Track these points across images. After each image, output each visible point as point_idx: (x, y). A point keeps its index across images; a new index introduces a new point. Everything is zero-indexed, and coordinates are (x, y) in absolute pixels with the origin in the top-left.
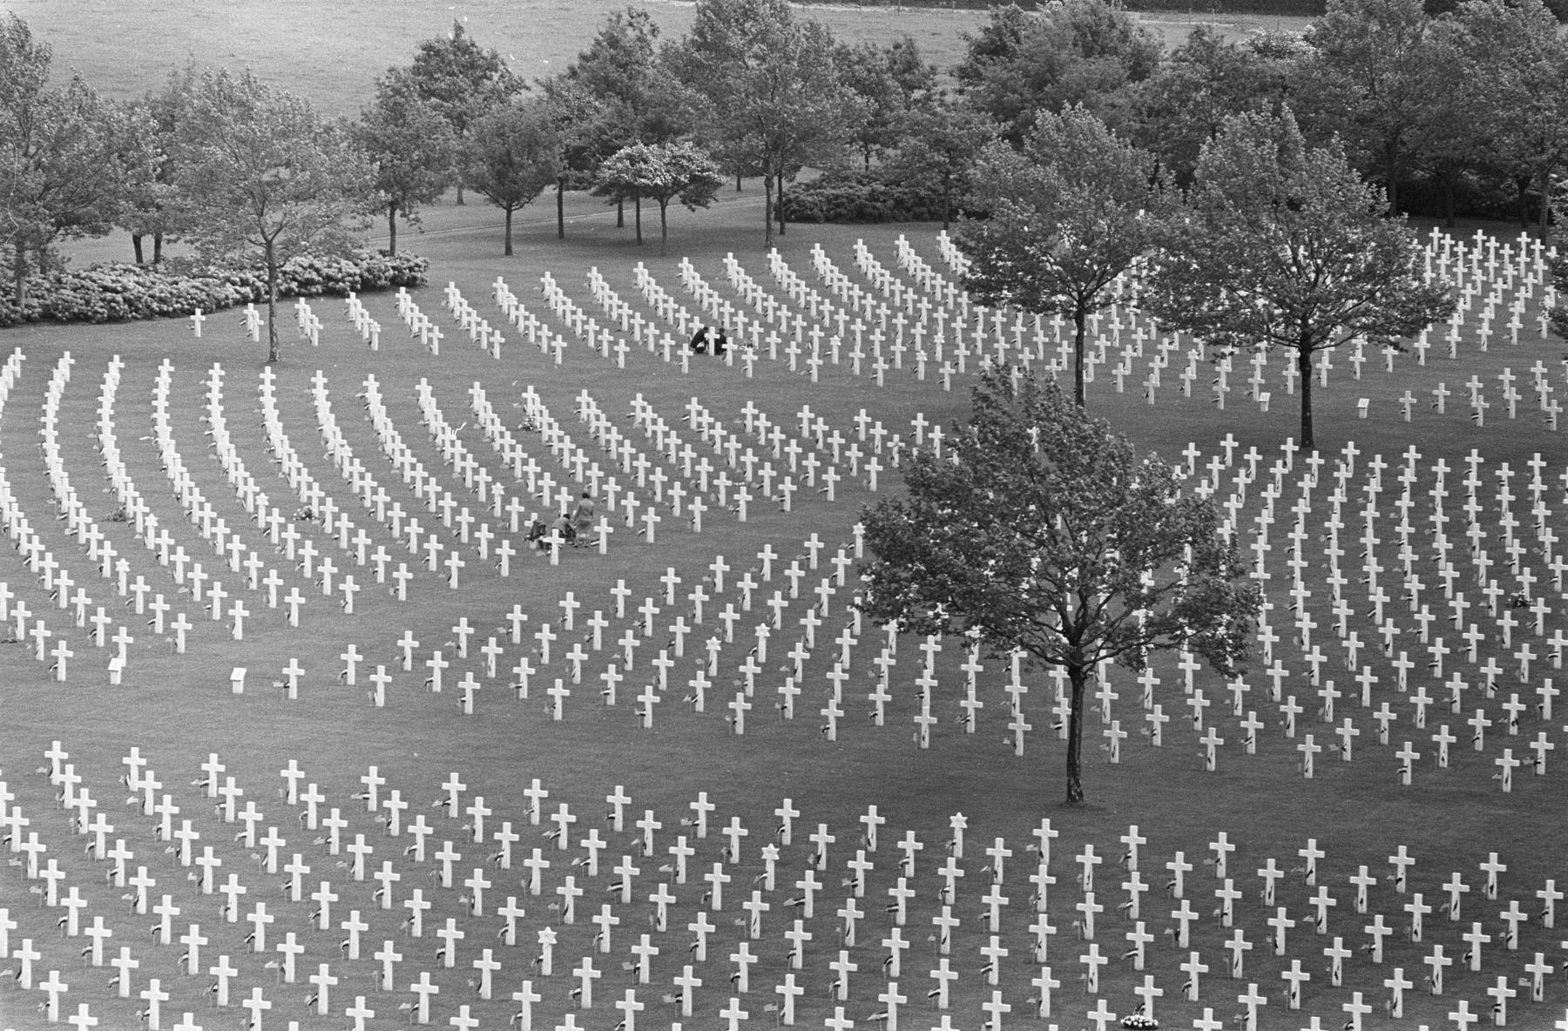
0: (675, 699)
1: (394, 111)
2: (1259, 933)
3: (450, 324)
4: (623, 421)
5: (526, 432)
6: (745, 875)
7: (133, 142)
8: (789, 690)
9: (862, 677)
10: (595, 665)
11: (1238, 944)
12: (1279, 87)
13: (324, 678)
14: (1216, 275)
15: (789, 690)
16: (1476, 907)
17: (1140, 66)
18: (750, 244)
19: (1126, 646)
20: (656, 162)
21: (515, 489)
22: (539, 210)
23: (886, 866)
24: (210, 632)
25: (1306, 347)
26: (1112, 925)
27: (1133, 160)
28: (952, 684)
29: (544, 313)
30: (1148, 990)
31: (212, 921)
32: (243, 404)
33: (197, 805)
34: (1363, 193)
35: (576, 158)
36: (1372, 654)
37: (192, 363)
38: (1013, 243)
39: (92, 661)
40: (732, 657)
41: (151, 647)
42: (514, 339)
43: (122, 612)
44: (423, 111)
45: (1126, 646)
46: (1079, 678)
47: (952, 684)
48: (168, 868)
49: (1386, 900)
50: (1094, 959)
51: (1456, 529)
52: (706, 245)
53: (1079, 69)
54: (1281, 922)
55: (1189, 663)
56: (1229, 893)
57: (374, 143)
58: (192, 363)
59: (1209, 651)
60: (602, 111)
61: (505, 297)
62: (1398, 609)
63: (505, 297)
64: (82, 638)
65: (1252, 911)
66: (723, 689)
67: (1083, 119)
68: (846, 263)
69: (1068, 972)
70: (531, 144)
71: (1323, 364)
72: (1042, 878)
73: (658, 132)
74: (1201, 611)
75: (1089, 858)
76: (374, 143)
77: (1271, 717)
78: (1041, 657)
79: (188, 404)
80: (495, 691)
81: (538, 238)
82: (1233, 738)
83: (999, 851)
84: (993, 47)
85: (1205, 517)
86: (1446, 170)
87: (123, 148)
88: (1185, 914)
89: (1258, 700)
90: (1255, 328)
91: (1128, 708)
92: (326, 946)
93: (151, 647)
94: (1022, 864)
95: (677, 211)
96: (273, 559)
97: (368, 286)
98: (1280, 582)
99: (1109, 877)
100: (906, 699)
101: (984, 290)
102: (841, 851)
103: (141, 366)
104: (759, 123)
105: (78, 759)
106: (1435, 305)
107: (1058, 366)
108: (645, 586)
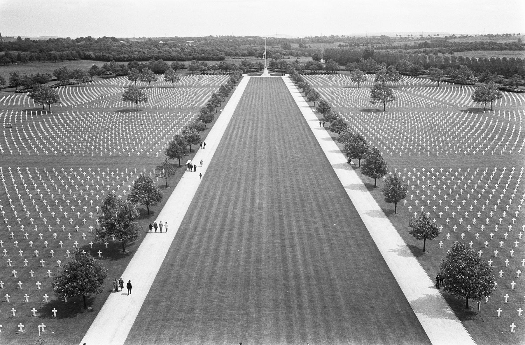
0: (112, 106)
1: (91, 70)
2: (149, 118)
3: (96, 83)
4: (104, 89)
5: (101, 90)
6: (117, 117)
7: (74, 73)
8: (119, 105)
9: (124, 104)
10: (107, 105)
11: (154, 119)
12: (147, 66)
13: (89, 107)
14: (144, 78)
15: (119, 105)
16: (162, 115)
17: (138, 65)
18: (115, 77)
19: (140, 101)
20: (108, 73)
21: (101, 94)
22: (101, 76)
23: (126, 116)
24: (82, 104)
25: (150, 82)
26: (140, 118)
27: (138, 71)
28: (129, 104)
29: (102, 82)
30: (143, 122)
31: (84, 122)
32: (83, 89)
33: (77, 116)
34: (152, 72)
35: (103, 73)
36: (155, 101)
37: (79, 87)
38: (131, 76)
39: (74, 106)
40: (115, 103)
41: (78, 105)
42: (100, 84)
43: (76, 103)
44: (92, 70)
45: (140, 101)
46: (137, 103)
47: (129, 104)
48: (80, 119)
49: (415, 115)
50: (139, 120)
51: (160, 93)
52: (112, 77)
53: (134, 65)
54: (150, 117)
55: (144, 102)
56: (147, 116)
57: (89, 72)
58: (79, 87)
59: (145, 101)
60: (104, 70)
61: (99, 81)
62: (156, 98)
63: (99, 81)
64: (74, 105)
65: (149, 117)
66: (121, 105)
67: (134, 68)
68: (121, 78)
69: (138, 121)
70: (100, 72)
71: (151, 83)
72: (136, 116)
73: (108, 71)
74: (145, 99)
75: (397, 114)
76: (89, 72)
77: (149, 105)
78: (135, 102)
79: (79, 90)
80: (101, 106)
81: (101, 78)
82: (147, 106)
83: (138, 114)
84: (129, 64)
85: (144, 93)
86: (158, 70)
87: (73, 73)
88: (150, 117)
89: (148, 104)
90: (146, 81)
91: (140, 105)
92: (91, 123)
93: (78, 105)
94: (134, 115)
95: (110, 76)
96: (86, 99)
97: (90, 81)
98: (149, 97)
99: (140, 115)
100: (126, 106)
101: (129, 80)
102: (123, 115)
103: (73, 87)
104: (114, 70)
105: (74, 112)
106: (157, 79)
107: (135, 84)
108: (110, 99)
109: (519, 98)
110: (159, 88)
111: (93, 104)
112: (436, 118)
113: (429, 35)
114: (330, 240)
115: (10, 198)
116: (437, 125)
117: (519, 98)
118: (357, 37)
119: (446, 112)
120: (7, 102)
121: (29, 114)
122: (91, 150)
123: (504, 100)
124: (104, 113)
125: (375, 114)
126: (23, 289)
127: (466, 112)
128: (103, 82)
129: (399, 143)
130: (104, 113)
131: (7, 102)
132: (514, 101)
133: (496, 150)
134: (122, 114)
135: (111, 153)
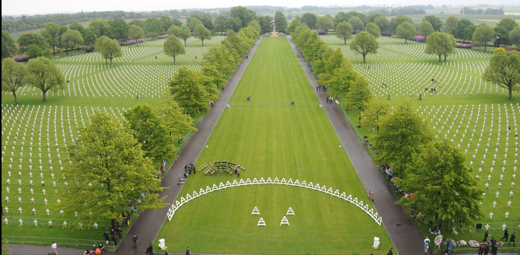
108: (159, 54)
109: (470, 54)
110: (195, 47)
111: (142, 59)
112: (403, 68)
113: (400, 6)
114: (65, 149)
115: (517, 131)
116: (404, 73)
117: (470, 54)
118: (125, 12)
119: (407, 63)
120: (85, 58)
121: (96, 67)
122: (145, 94)
123: (458, 55)
124: (157, 66)
125: (163, 67)
126: (497, 198)
127: (418, 63)
128: (151, 43)
129: (147, 86)
130: (157, 66)
131: (85, 58)
132: (465, 55)
133: (25, 90)
134: (171, 67)
135: (153, 96)
